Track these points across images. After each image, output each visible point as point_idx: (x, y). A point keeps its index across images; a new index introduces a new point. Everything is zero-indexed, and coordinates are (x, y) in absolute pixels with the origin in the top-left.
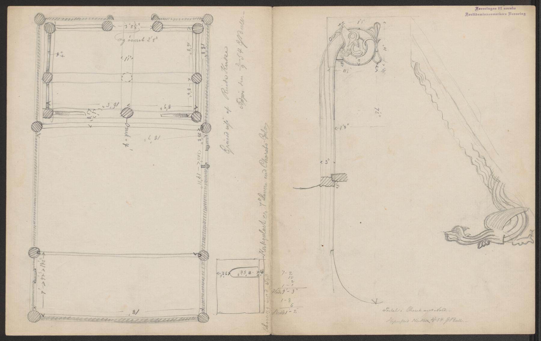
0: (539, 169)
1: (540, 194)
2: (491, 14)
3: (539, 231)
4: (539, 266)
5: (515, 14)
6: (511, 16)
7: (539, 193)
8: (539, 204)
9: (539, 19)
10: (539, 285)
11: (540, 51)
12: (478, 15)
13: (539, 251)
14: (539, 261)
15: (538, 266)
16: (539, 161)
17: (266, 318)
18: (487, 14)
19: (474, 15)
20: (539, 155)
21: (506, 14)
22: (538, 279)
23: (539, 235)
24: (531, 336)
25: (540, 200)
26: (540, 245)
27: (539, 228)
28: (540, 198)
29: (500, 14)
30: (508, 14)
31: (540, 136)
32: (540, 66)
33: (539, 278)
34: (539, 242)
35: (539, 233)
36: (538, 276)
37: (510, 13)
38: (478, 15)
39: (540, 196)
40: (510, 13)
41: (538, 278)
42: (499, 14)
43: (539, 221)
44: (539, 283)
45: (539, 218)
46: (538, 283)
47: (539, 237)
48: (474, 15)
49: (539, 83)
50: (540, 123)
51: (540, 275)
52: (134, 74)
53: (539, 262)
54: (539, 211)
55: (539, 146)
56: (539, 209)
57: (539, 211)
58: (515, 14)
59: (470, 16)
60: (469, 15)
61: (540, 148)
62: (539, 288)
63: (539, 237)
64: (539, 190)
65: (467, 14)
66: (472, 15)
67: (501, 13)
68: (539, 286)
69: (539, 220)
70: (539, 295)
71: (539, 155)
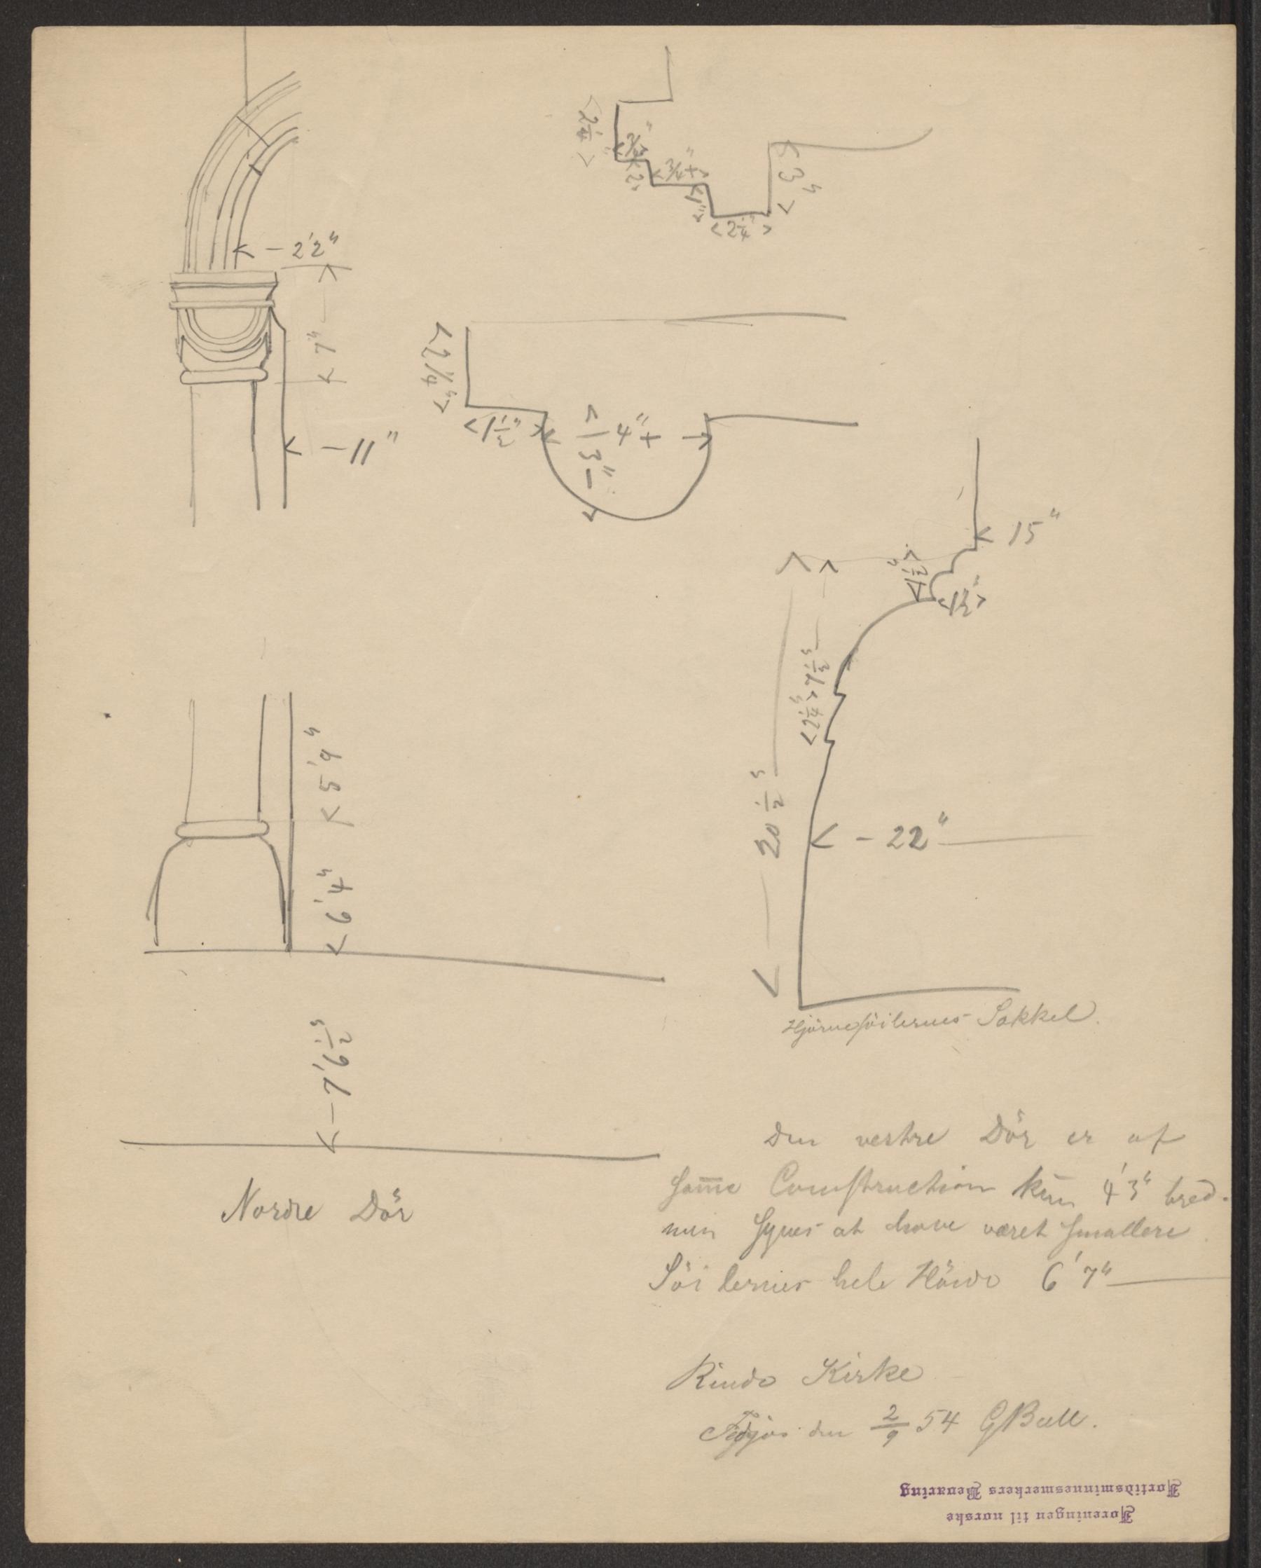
0: (1247, 975)
1: (1252, 1092)
2: (1059, 1490)
3: (1251, 1264)
4: (1251, 1425)
5: (951, 1491)
6: (968, 1484)
7: (1251, 1085)
8: (1251, 1137)
9: (1250, 280)
10: (1250, 1511)
11: (1253, 427)
12: (1119, 1489)
13: (1247, 1353)
14: (1247, 1403)
15: (1246, 1424)
16: (1252, 937)
17: (732, 1382)
18: (1078, 1489)
19: (1141, 1489)
20: (1251, 908)
21: (992, 1491)
22: (1245, 1486)
23: (1251, 1281)
24: (1211, 1548)
25: (1251, 1118)
26: (1252, 1325)
27: (1251, 1252)
28: (1252, 1111)
29: (1019, 1490)
30: (984, 1491)
31: (1252, 823)
32: (1254, 498)
33: (1250, 1479)
34: (1251, 1313)
35: (1247, 1273)
36: (1246, 1473)
37: (973, 1493)
38: (1119, 1489)
39: (1252, 1100)
40: (973, 1493)
41: (1247, 1478)
42: (1024, 1490)
43: (1251, 1214)
44: (1250, 1502)
45: (1251, 1202)
46: (1246, 1507)
47: (1251, 1288)
48: (1141, 1489)
49: (1249, 575)
50: (1252, 762)
51: (1255, 1467)
52: (259, 140)
53: (1251, 1407)
54: (1251, 1172)
55: (1248, 871)
56: (1247, 1163)
57: (1247, 1169)
58: (951, 1491)
59: (1157, 1483)
60: (1161, 1488)
61: (1252, 880)
62: (1250, 1528)
63: (1247, 1292)
64: (1251, 1073)
65: (1173, 1491)
66: (1148, 1488)
67: (1015, 1496)
68: (1251, 1519)
69: (1247, 1212)
70: (1250, 1561)
71: (1247, 913)
